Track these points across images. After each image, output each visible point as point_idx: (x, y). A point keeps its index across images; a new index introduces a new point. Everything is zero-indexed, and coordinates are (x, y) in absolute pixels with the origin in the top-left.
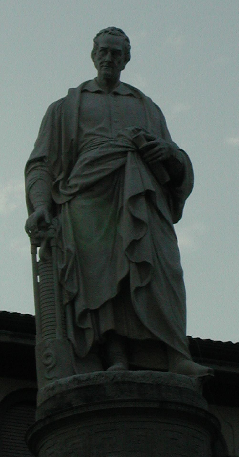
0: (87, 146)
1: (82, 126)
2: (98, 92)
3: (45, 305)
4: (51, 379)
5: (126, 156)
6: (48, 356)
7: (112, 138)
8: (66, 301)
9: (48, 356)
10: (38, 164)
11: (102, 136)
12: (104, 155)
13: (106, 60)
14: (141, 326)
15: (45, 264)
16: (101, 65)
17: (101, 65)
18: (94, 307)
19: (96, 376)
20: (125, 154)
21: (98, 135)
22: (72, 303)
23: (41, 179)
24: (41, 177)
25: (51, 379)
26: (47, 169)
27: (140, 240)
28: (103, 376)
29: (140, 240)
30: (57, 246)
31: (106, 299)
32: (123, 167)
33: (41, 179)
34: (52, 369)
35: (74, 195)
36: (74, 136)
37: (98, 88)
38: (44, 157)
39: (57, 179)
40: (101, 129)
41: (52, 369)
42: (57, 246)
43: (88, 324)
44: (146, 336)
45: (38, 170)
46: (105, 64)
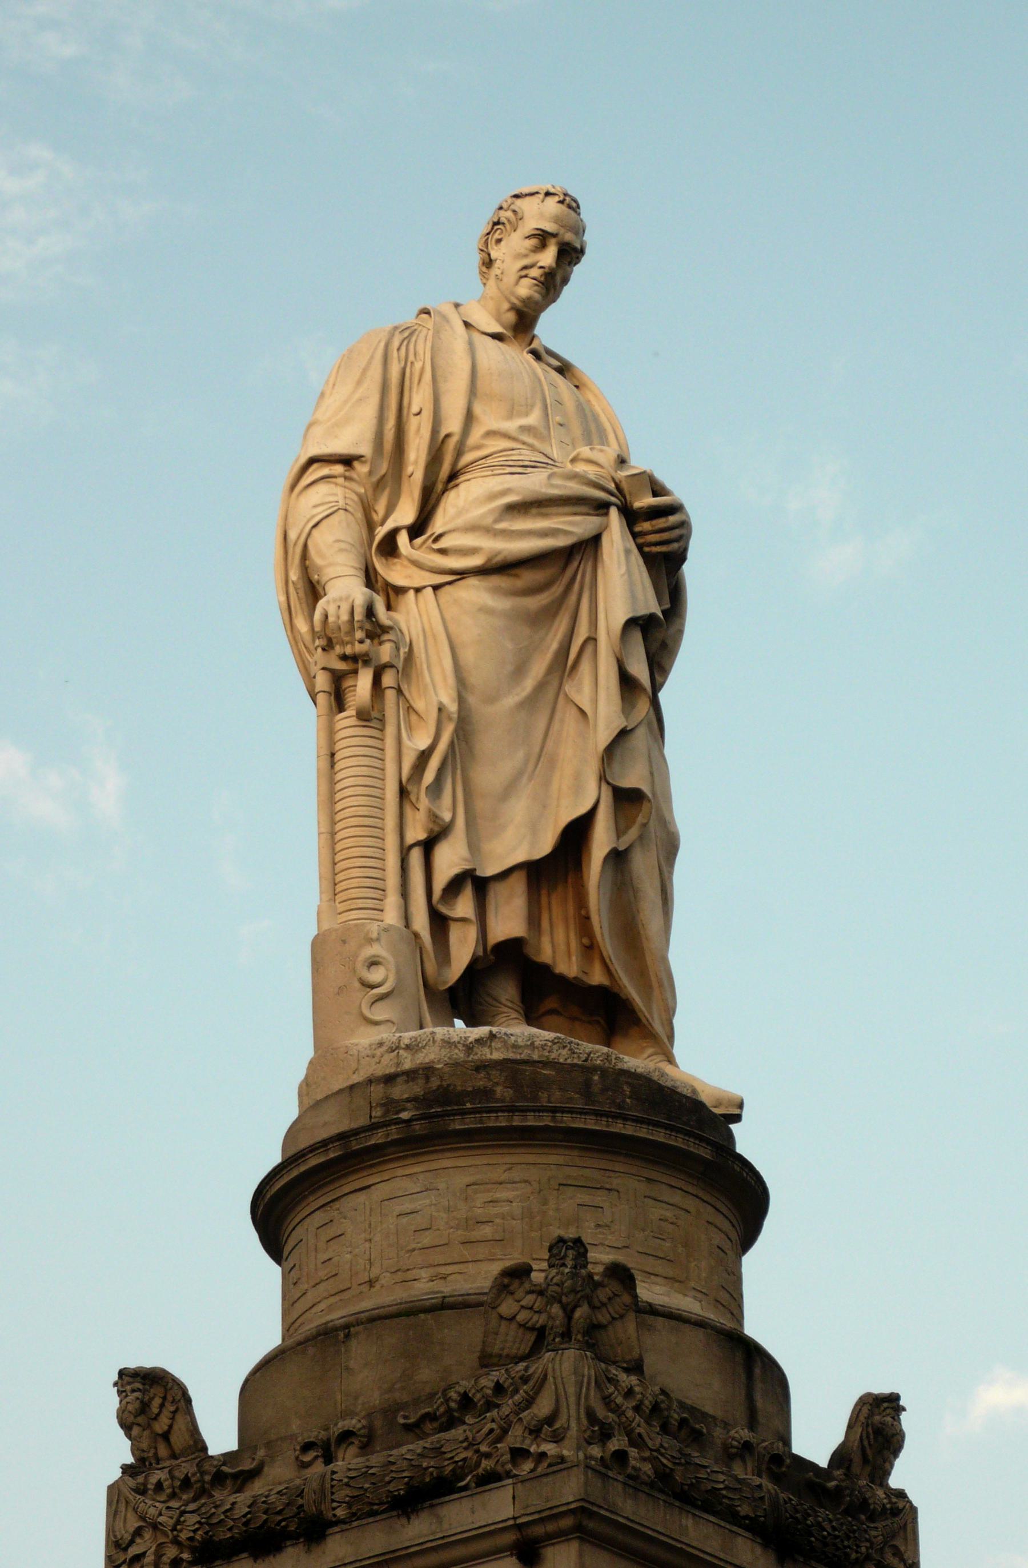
0: (489, 461)
1: (478, 409)
2: (497, 337)
3: (355, 883)
4: (376, 1023)
5: (607, 514)
6: (373, 963)
7: (555, 461)
8: (416, 833)
9: (373, 963)
10: (339, 469)
11: (532, 448)
12: (561, 496)
13: (540, 264)
14: (590, 948)
15: (364, 726)
16: (524, 273)
17: (524, 273)
18: (490, 870)
19: (550, 1044)
20: (601, 508)
21: (524, 443)
22: (428, 846)
23: (346, 510)
24: (346, 504)
25: (376, 1023)
26: (362, 491)
27: (632, 730)
28: (564, 1047)
29: (632, 730)
30: (399, 691)
31: (520, 856)
32: (594, 542)
33: (346, 510)
34: (382, 997)
35: (462, 574)
36: (453, 425)
37: (498, 329)
38: (359, 458)
39: (390, 525)
40: (526, 429)
41: (382, 997)
42: (399, 691)
43: (464, 906)
44: (597, 977)
45: (336, 484)
46: (535, 272)
